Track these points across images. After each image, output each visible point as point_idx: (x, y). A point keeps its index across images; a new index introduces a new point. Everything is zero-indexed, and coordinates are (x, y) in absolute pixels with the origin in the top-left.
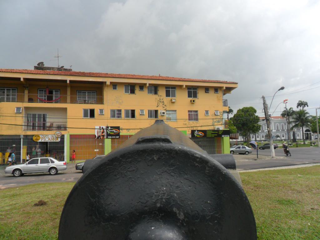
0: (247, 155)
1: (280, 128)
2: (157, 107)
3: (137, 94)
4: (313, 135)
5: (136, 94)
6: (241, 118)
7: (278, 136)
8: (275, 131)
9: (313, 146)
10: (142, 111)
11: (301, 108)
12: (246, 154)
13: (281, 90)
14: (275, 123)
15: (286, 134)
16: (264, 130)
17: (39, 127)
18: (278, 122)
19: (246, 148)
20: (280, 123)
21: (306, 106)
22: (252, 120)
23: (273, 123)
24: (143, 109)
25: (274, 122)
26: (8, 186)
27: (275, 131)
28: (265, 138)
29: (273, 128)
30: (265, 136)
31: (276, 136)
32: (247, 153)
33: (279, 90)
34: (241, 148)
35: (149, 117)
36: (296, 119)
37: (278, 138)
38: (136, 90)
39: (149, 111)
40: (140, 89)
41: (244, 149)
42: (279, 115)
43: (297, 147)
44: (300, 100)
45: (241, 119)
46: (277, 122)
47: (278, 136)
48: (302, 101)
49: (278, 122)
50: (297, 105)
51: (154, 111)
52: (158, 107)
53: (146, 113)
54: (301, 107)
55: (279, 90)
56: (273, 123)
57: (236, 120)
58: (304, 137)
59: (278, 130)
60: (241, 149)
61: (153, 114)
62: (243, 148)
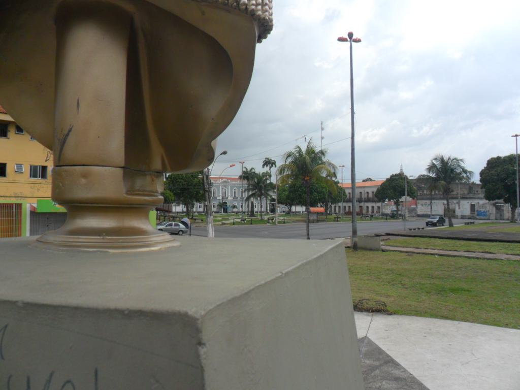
0: (181, 235)
1: (238, 195)
2: (46, 161)
3: (10, 137)
4: (279, 207)
5: (9, 138)
6: (180, 180)
7: (234, 207)
8: (232, 198)
9: (270, 223)
10: (19, 166)
11: (266, 169)
12: (180, 235)
13: (223, 155)
14: (232, 188)
15: (258, 203)
16: (216, 196)
17: (308, 235)
18: (236, 187)
19: (179, 226)
20: (238, 187)
21: (274, 166)
22: (196, 184)
23: (229, 187)
24: (22, 163)
25: (231, 186)
26: (79, 238)
27: (232, 198)
28: (217, 208)
29: (229, 194)
30: (217, 206)
31: (232, 205)
32: (181, 233)
33: (221, 154)
34: (173, 225)
35: (31, 177)
36: (253, 186)
37: (235, 210)
38: (9, 131)
39: (31, 166)
40: (18, 131)
41: (177, 227)
42: (237, 177)
43: (251, 224)
44: (267, 157)
45: (181, 182)
46: (235, 187)
47: (234, 207)
48: (270, 159)
49: (236, 187)
50: (262, 164)
51: (40, 167)
52: (48, 161)
53: (26, 169)
54: (267, 166)
55: (221, 154)
56: (229, 187)
57: (173, 182)
58: (268, 208)
59: (235, 198)
60: (173, 227)
61: (39, 172)
62: (176, 225)
